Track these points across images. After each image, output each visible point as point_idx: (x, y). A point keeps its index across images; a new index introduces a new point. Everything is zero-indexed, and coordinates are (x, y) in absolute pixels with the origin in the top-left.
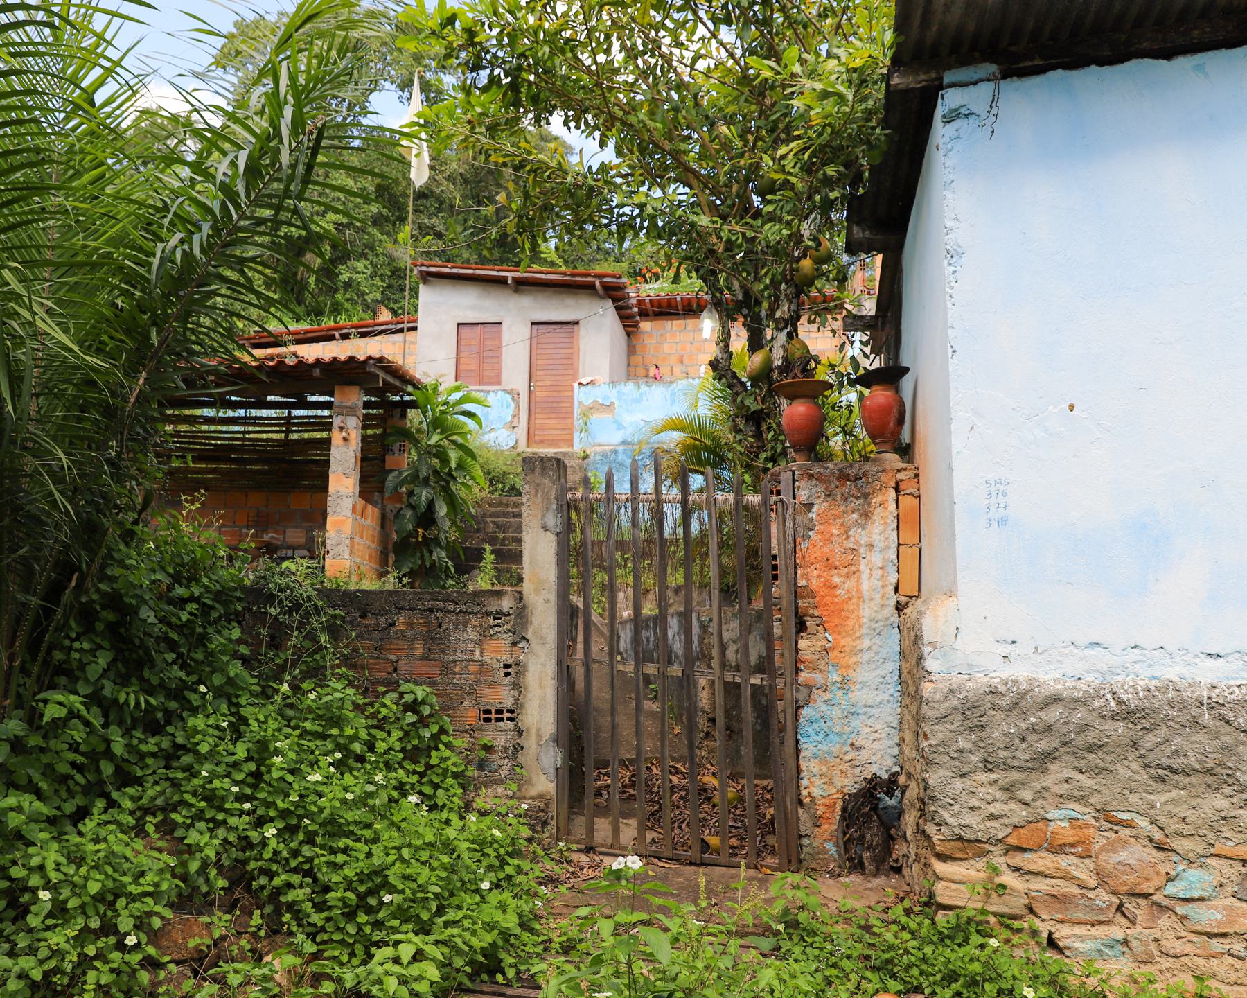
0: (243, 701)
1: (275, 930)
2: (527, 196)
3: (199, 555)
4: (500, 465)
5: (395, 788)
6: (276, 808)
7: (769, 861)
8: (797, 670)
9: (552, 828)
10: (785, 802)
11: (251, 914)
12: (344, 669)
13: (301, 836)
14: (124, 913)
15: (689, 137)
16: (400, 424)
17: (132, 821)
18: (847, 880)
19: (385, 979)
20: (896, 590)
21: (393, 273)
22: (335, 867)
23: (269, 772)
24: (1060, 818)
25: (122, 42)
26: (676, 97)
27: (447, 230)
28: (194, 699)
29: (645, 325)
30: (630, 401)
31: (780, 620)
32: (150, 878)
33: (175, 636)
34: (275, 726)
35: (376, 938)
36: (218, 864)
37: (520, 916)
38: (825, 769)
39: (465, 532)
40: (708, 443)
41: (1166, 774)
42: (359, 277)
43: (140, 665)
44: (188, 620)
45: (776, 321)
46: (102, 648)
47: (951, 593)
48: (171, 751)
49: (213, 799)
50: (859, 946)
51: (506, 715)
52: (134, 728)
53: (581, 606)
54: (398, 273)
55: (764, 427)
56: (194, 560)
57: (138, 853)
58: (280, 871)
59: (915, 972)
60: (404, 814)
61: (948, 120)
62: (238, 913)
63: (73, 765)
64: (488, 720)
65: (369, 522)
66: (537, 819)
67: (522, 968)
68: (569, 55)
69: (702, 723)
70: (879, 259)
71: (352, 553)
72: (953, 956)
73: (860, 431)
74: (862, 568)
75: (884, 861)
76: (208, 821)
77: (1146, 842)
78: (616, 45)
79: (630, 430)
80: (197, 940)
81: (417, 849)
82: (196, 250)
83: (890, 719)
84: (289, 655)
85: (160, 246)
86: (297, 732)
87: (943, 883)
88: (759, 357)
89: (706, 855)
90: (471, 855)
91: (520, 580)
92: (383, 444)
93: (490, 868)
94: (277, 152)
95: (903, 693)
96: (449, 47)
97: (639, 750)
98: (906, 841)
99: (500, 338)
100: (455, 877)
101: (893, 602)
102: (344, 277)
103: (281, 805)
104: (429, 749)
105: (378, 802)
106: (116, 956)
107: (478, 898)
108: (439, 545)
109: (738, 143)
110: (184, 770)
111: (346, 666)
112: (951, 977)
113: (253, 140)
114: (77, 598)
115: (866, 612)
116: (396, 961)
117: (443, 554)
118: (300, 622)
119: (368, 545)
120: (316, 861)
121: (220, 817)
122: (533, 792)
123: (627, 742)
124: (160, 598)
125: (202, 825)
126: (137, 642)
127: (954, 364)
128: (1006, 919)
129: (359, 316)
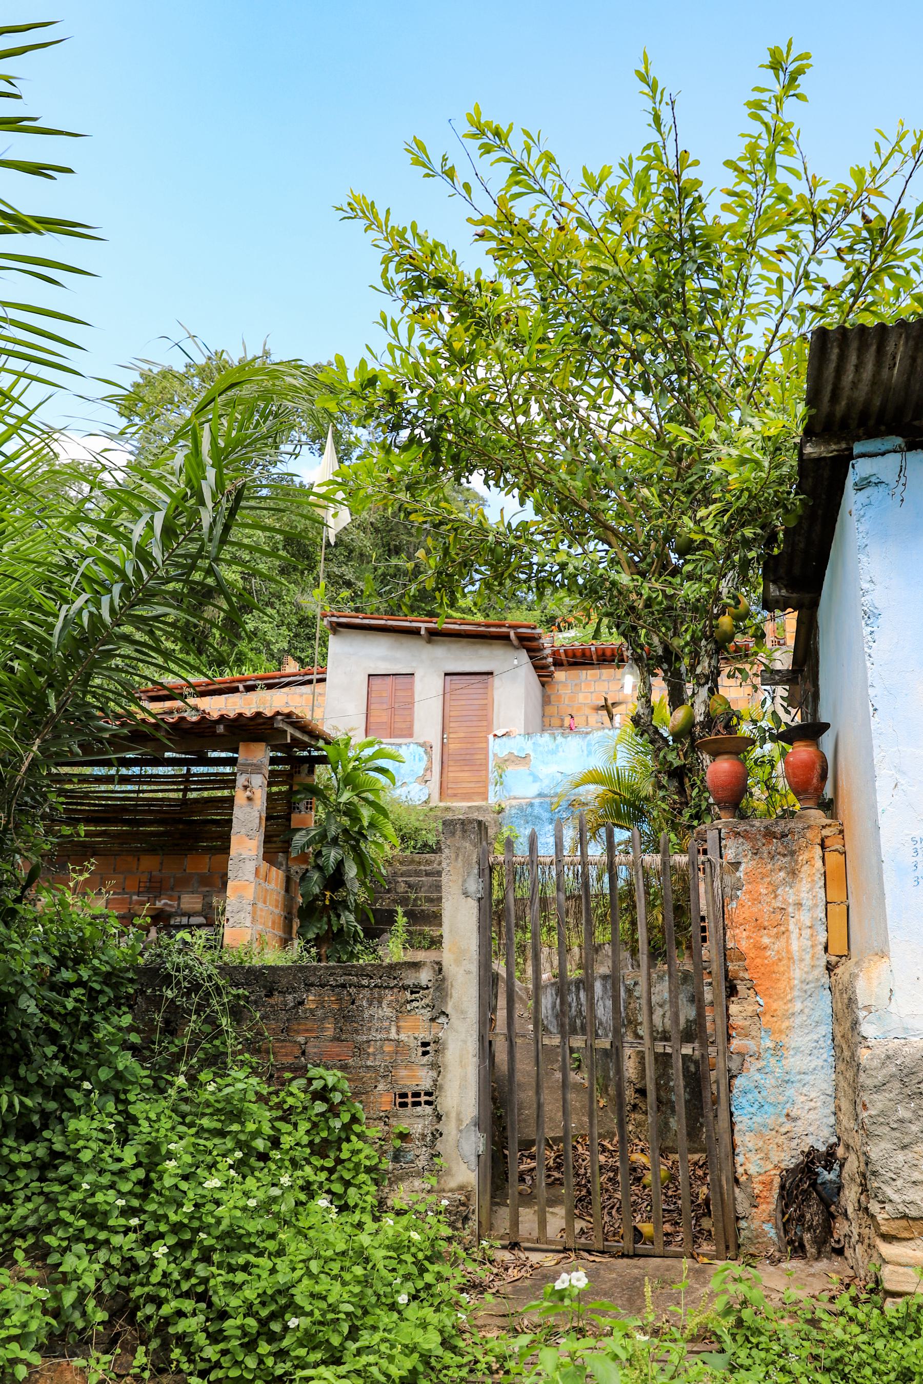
0: (131, 1097)
2: (446, 551)
3: (88, 934)
5: (302, 1188)
6: (167, 1222)
7: (706, 1247)
8: (729, 1037)
9: (473, 1224)
10: (720, 1181)
11: (133, 1352)
12: (247, 1055)
13: (195, 1253)
16: (308, 780)
20: (826, 949)
21: (300, 622)
22: (233, 1287)
23: (160, 1178)
25: (30, 400)
26: (593, 456)
27: (357, 578)
28: (77, 1098)
29: (560, 675)
31: (710, 984)
32: (17, 1317)
33: (56, 1026)
34: (169, 1126)
36: (98, 1294)
37: (441, 1332)
38: (760, 1144)
39: (376, 891)
40: (628, 796)
42: (266, 627)
43: (15, 1061)
44: (75, 1008)
45: (697, 677)
47: (883, 954)
48: (47, 1159)
49: (93, 1215)
51: (423, 1098)
54: (306, 622)
55: (687, 785)
56: (82, 940)
58: (170, 1296)
60: (312, 1220)
61: (859, 487)
62: (118, 1351)
64: (403, 1105)
65: (272, 886)
66: (458, 1216)
68: (490, 417)
69: (629, 1095)
71: (254, 920)
72: (905, 1351)
73: (782, 784)
74: (792, 927)
75: (825, 1242)
76: (87, 1242)
79: (546, 782)
83: (824, 1086)
85: (65, 607)
87: (890, 1267)
88: (681, 713)
89: (638, 1246)
90: (387, 1262)
92: (289, 802)
93: (407, 1277)
95: (836, 1058)
96: (370, 406)
97: (566, 1128)
98: (847, 1219)
99: (411, 689)
100: (369, 1291)
102: (250, 627)
103: (173, 1218)
104: (340, 1141)
105: (284, 1208)
107: (395, 1316)
108: (347, 908)
110: (62, 1182)
111: (248, 1051)
112: (905, 1375)
113: (168, 500)
115: (797, 973)
117: (352, 918)
118: (199, 1004)
119: (271, 910)
120: (212, 1282)
121: (102, 1236)
122: (453, 1184)
123: (551, 1119)
125: (80, 1248)
126: (14, 1035)
129: (267, 668)
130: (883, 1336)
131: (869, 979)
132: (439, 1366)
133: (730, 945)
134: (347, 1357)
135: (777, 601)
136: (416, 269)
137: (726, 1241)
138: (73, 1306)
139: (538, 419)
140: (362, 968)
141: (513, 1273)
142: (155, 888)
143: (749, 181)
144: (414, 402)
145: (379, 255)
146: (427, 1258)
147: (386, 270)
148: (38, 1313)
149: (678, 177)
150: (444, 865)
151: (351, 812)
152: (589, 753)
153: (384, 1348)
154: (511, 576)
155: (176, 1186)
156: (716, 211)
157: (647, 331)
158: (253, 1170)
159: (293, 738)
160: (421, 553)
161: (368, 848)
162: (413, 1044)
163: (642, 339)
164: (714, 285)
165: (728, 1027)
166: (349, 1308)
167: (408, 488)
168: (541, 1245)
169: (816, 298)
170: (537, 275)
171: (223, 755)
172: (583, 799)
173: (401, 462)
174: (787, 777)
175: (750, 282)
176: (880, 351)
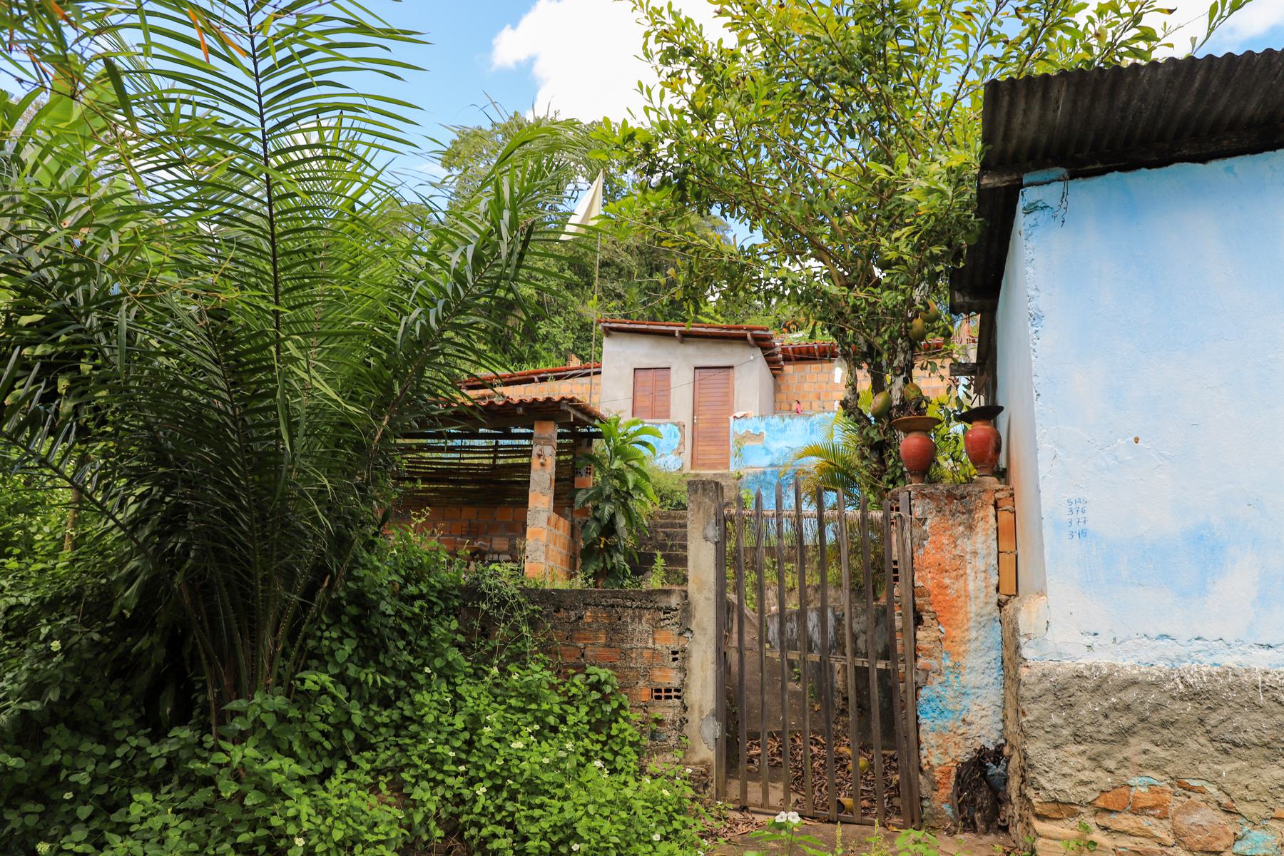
0: (458, 681)
4: (669, 485)
5: (582, 754)
7: (895, 820)
8: (916, 657)
9: (712, 789)
13: (505, 794)
16: (588, 451)
20: (998, 589)
22: (533, 820)
23: (480, 740)
24: (1140, 784)
25: (377, 164)
28: (421, 679)
29: (789, 369)
33: (406, 627)
34: (486, 702)
36: (437, 818)
40: (841, 466)
41: (1231, 747)
42: (555, 331)
45: (894, 369)
47: (1042, 593)
48: (399, 722)
49: (436, 762)
54: (586, 327)
60: (590, 776)
61: (1028, 211)
64: (659, 698)
65: (561, 532)
66: (699, 782)
68: (725, 161)
71: (547, 558)
74: (969, 571)
75: (993, 821)
76: (429, 780)
77: (1215, 806)
79: (776, 455)
83: (995, 698)
88: (880, 399)
93: (660, 822)
95: (1005, 677)
100: (632, 830)
101: (995, 600)
102: (543, 331)
103: (489, 768)
104: (610, 722)
105: (568, 766)
115: (973, 608)
117: (622, 558)
119: (559, 551)
120: (517, 815)
121: (440, 777)
122: (696, 759)
126: (375, 631)
131: (1029, 612)
133: (918, 583)
135: (962, 307)
136: (670, 40)
146: (675, 811)
147: (646, 43)
148: (396, 826)
157: (853, 87)
160: (671, 271)
165: (916, 649)
169: (999, 50)
172: (806, 469)
173: (654, 199)
174: (967, 452)
175: (945, 39)
176: (1045, 97)
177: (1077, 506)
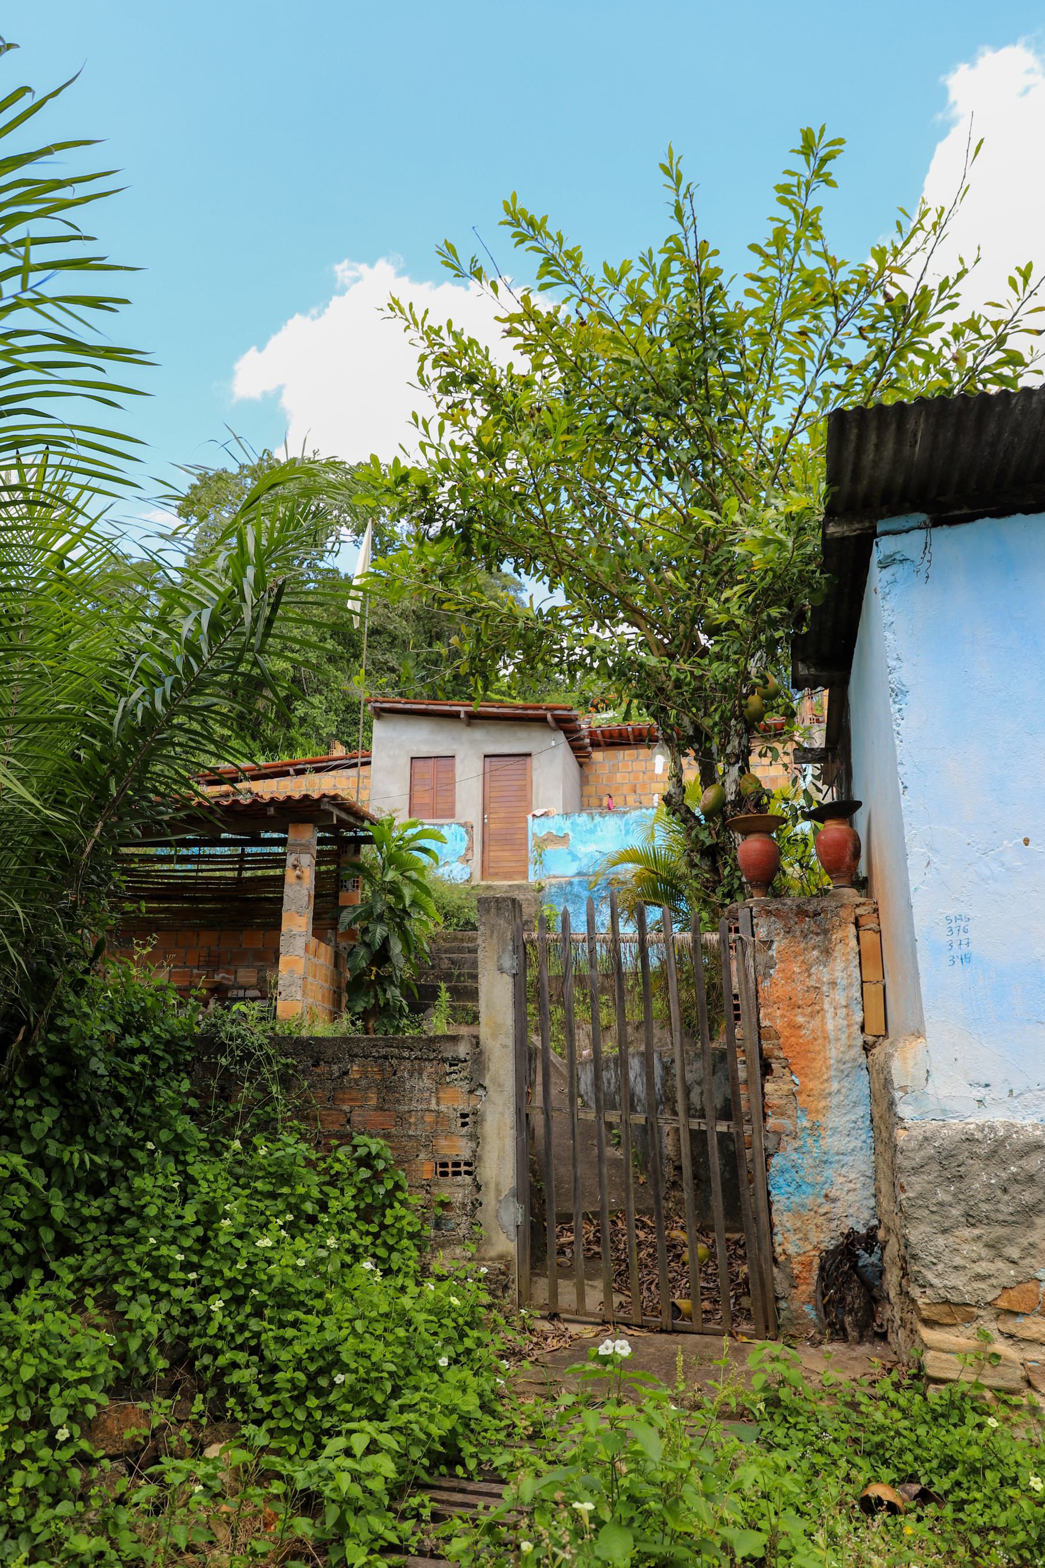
0: (190, 1158)
1: (217, 1414)
5: (348, 1251)
7: (745, 1327)
8: (765, 1116)
9: (513, 1293)
13: (248, 1309)
14: (57, 1402)
15: (636, 580)
16: (354, 859)
17: (71, 1296)
18: (829, 1348)
19: (337, 1475)
20: (862, 1029)
22: (284, 1342)
25: (92, 510)
26: (621, 542)
28: (142, 1157)
29: (598, 756)
30: (587, 834)
32: (86, 1361)
33: (123, 1090)
35: (326, 1425)
36: (160, 1343)
37: (481, 1396)
42: (315, 712)
43: (85, 1121)
45: (727, 756)
46: (49, 1104)
47: (919, 1034)
49: (158, 1267)
50: (845, 1426)
51: (463, 1168)
52: (77, 1189)
53: (539, 1045)
54: (352, 708)
56: (144, 1009)
57: (75, 1333)
59: (909, 1457)
60: (358, 1282)
61: (884, 565)
63: (13, 1233)
64: (444, 1174)
65: (322, 961)
66: (496, 1283)
67: (484, 1458)
70: (826, 692)
71: (304, 994)
72: (948, 1439)
74: (826, 1006)
76: (150, 1293)
78: (564, 496)
79: (585, 861)
80: (134, 1431)
81: (371, 1321)
82: (159, 706)
83: (864, 1167)
84: (240, 1107)
86: (247, 1192)
87: (932, 1353)
88: (711, 793)
91: (476, 1017)
93: (448, 1341)
94: (240, 609)
95: (876, 1140)
100: (412, 1353)
101: (860, 1042)
103: (228, 1274)
104: (384, 1207)
105: (330, 1269)
106: (45, 1453)
107: (436, 1377)
108: (392, 983)
109: (684, 586)
114: (23, 1051)
115: (833, 1053)
116: (348, 1452)
117: (397, 992)
120: (264, 1337)
121: (164, 1288)
122: (493, 1253)
124: (108, 1049)
125: (144, 1298)
126: (84, 1097)
127: (906, 801)
128: (1003, 1394)
129: (314, 752)
130: (925, 1422)
131: (905, 1059)
132: (478, 1429)
134: (390, 1414)
137: (766, 1321)
138: (138, 1352)
139: (568, 506)
140: (403, 1041)
141: (553, 1343)
142: (213, 963)
143: (775, 266)
144: (446, 497)
145: (418, 352)
147: (421, 369)
148: (106, 1357)
149: (698, 267)
150: (479, 941)
151: (394, 890)
152: (627, 833)
153: (423, 1407)
154: (542, 660)
155: (230, 1244)
156: (738, 295)
157: (669, 418)
158: (302, 1232)
159: (339, 819)
160: (454, 640)
161: (413, 926)
162: (453, 1115)
163: (667, 425)
164: (736, 368)
165: (764, 1106)
166: (392, 1368)
167: (441, 578)
168: (580, 1315)
169: (841, 377)
170: (561, 370)
171: (275, 835)
173: (432, 554)
175: (777, 364)
177: (958, 924)
